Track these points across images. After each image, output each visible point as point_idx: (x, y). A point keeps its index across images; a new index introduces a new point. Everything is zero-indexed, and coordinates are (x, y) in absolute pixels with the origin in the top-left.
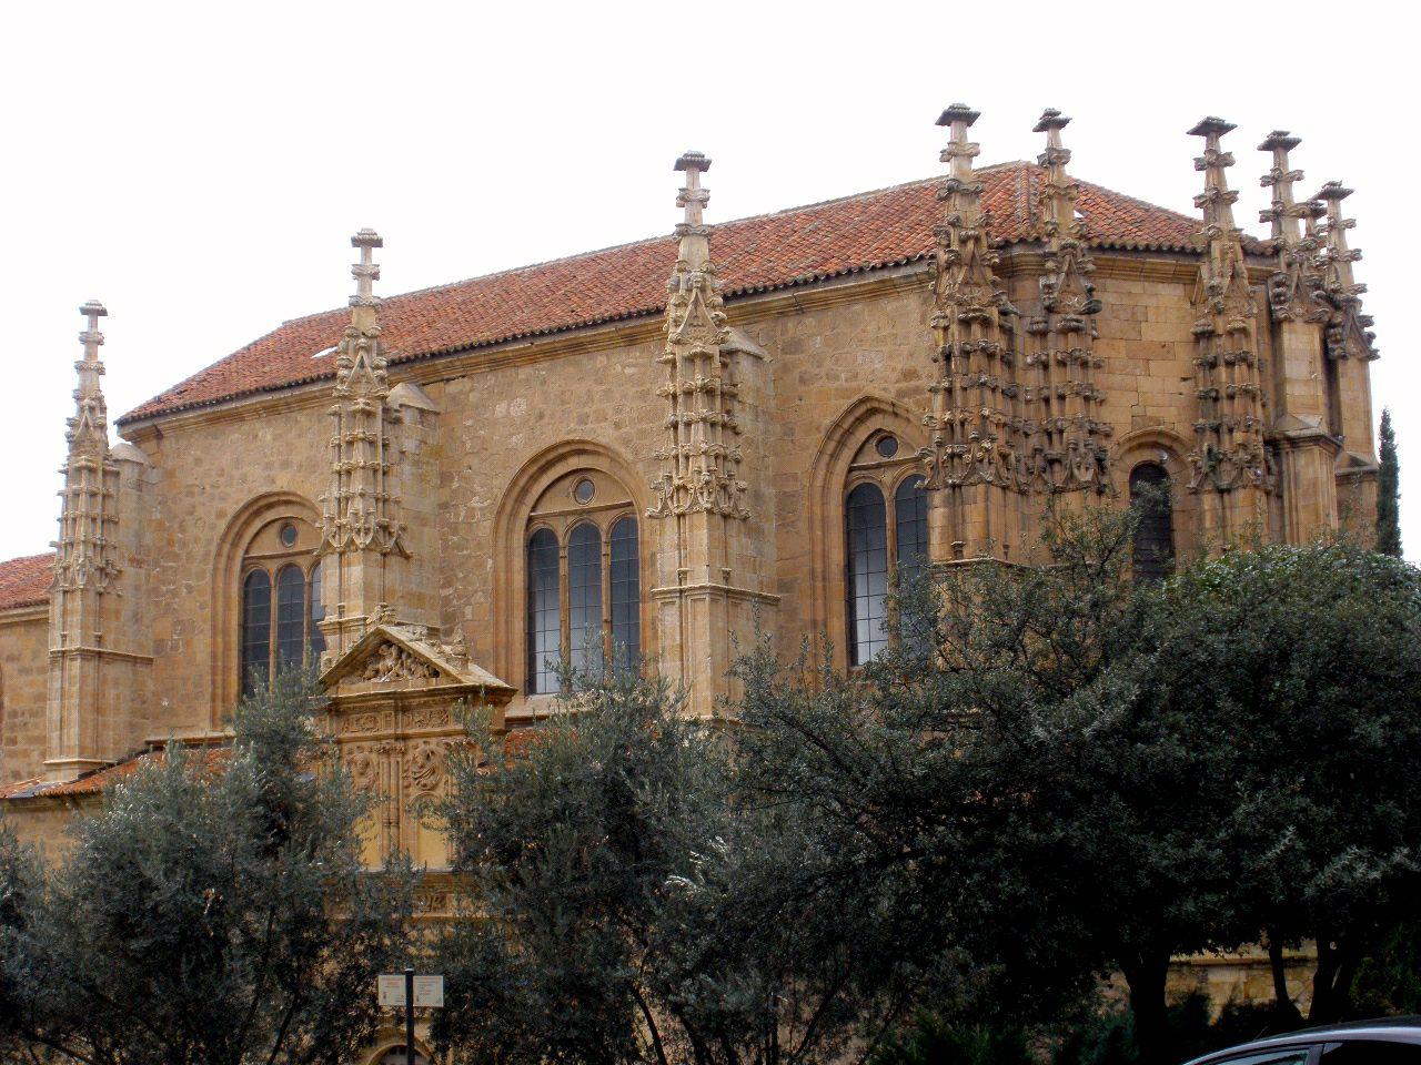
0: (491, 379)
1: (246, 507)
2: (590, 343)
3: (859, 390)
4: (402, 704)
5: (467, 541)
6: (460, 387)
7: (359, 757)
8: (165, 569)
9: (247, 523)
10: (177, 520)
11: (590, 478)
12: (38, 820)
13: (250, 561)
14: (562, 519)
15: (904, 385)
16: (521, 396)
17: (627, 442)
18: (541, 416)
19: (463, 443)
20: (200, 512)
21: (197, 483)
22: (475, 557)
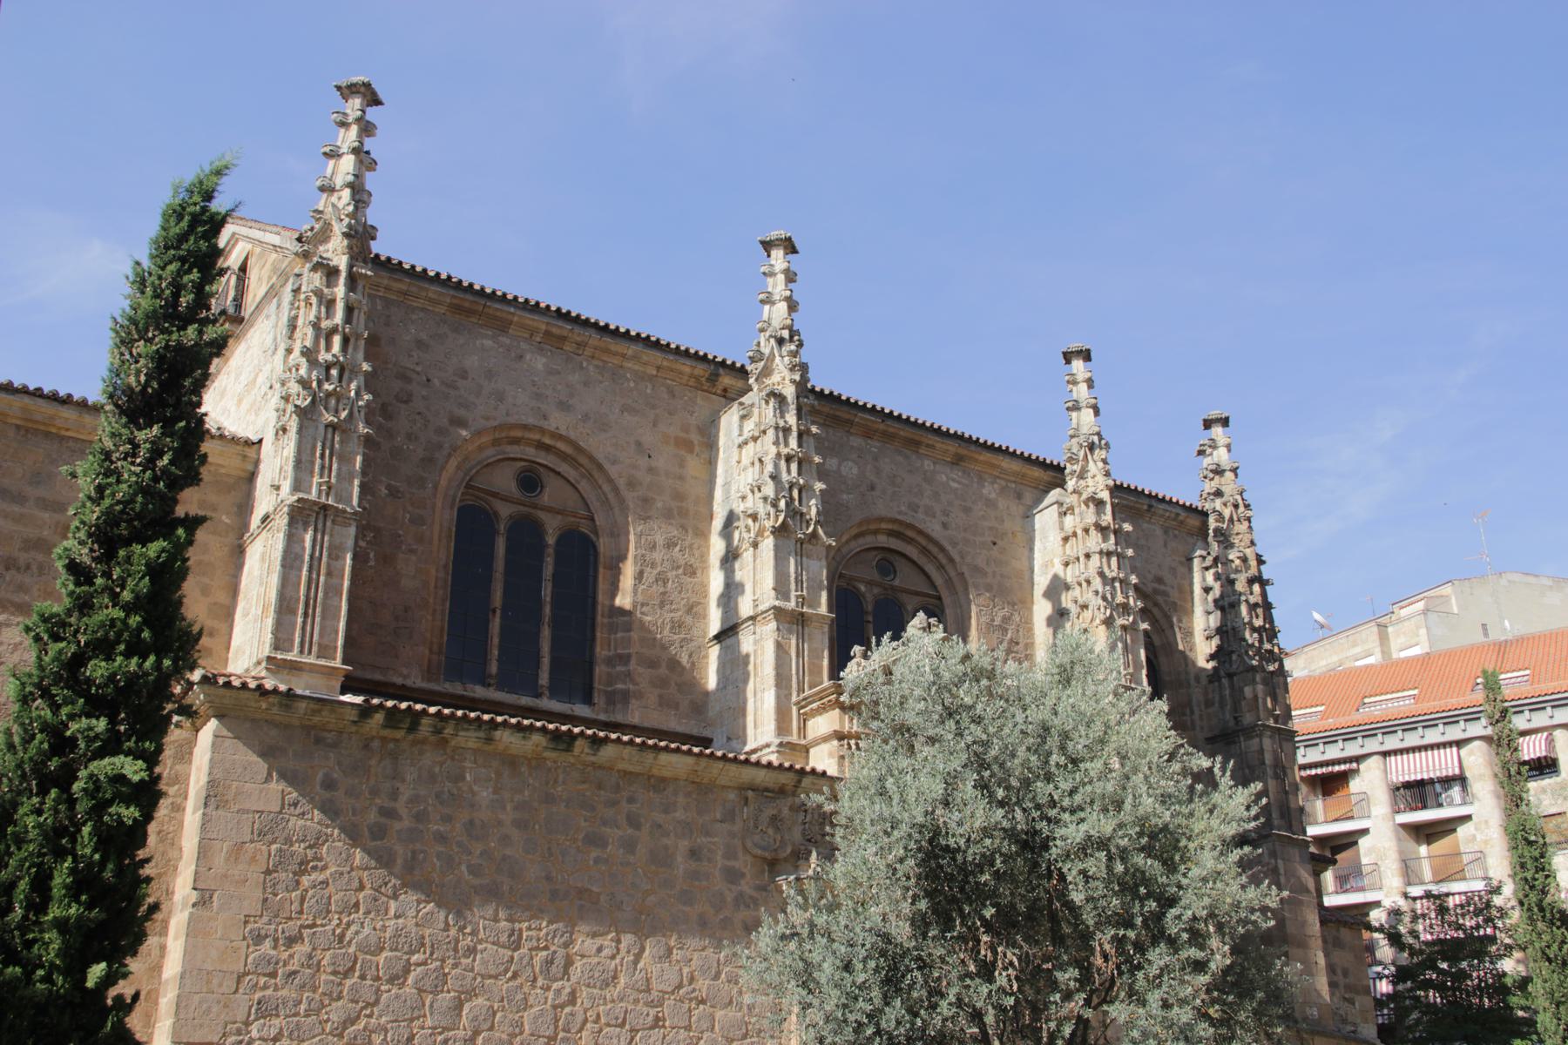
11: (896, 564)
15: (1156, 585)
16: (854, 461)
18: (872, 488)
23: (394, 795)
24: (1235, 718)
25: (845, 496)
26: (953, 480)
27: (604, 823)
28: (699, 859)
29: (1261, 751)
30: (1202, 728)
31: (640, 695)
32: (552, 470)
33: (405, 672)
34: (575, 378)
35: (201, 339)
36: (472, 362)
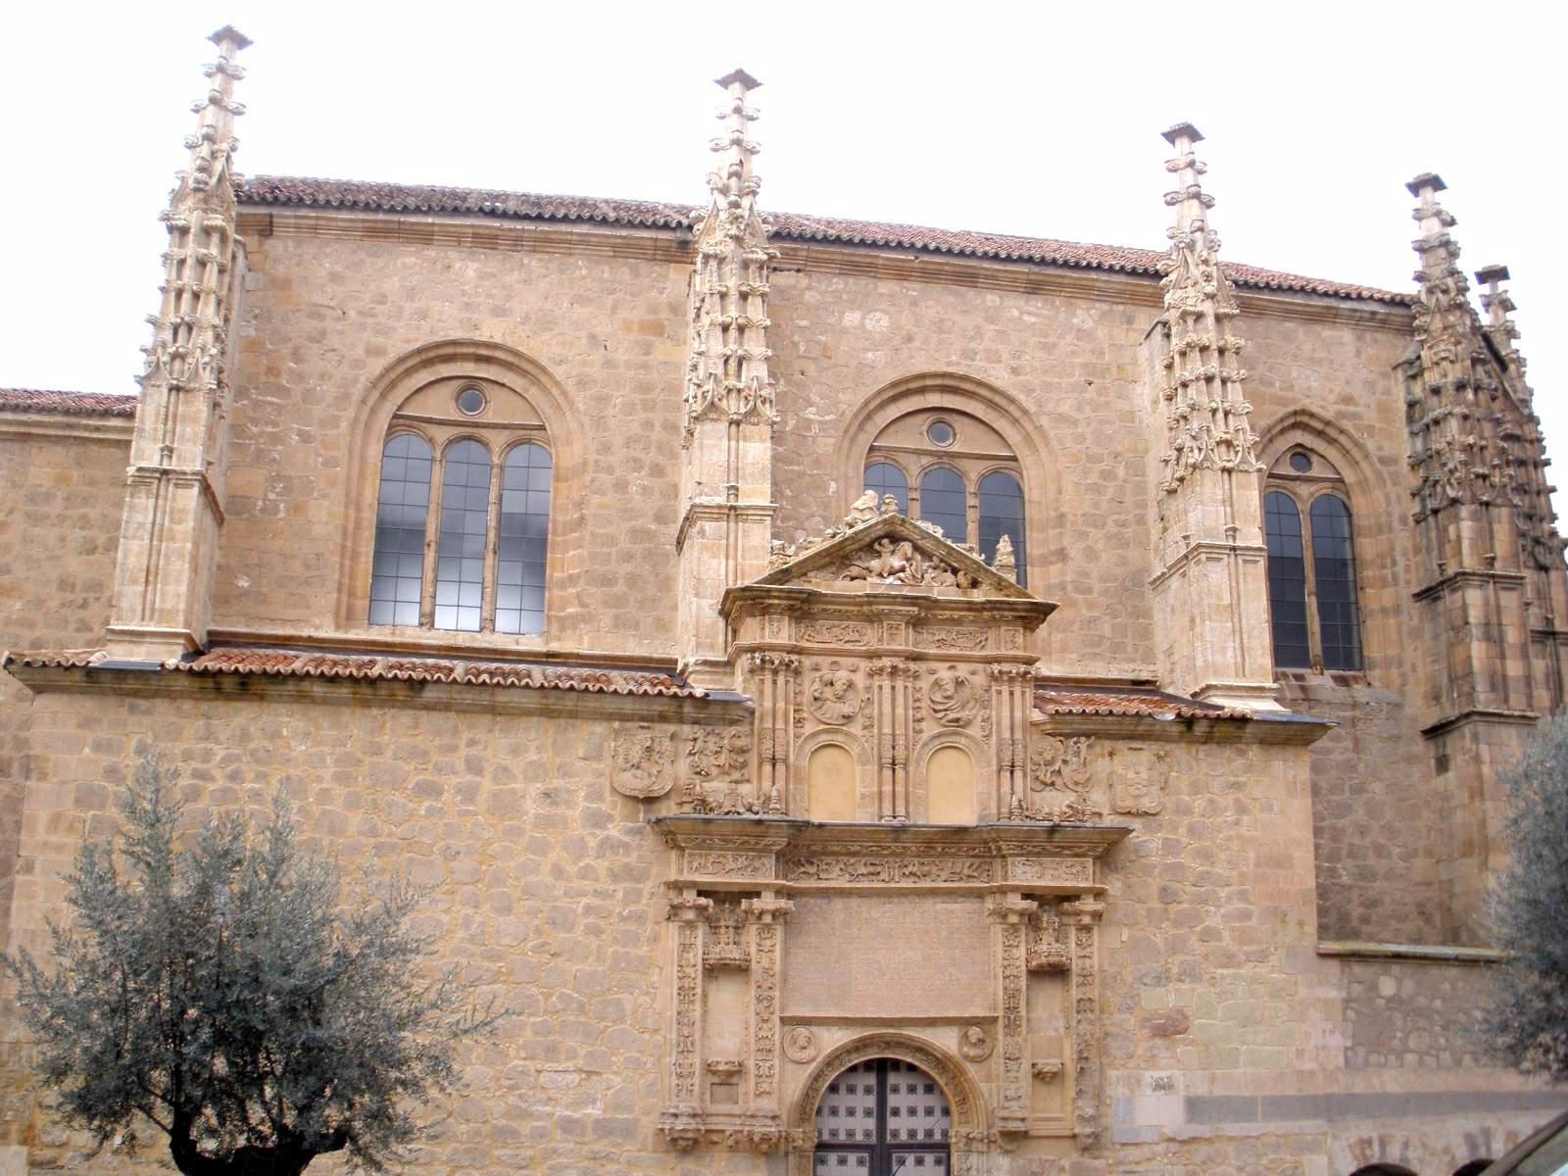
0: (838, 283)
1: (419, 351)
2: (986, 277)
3: (1294, 401)
4: (923, 613)
5: (800, 455)
6: (792, 281)
7: (842, 675)
8: (257, 405)
9: (409, 372)
10: (290, 345)
11: (956, 426)
12: (132, 709)
13: (401, 421)
14: (914, 457)
15: (1342, 407)
16: (882, 311)
17: (1029, 391)
18: (910, 339)
19: (795, 345)
20: (332, 340)
21: (332, 304)
22: (811, 476)
23: (207, 756)
24: (1440, 566)
25: (870, 355)
28: (554, 803)
29: (1464, 607)
30: (1408, 582)
32: (496, 382)
33: (317, 621)
34: (514, 277)
36: (392, 285)
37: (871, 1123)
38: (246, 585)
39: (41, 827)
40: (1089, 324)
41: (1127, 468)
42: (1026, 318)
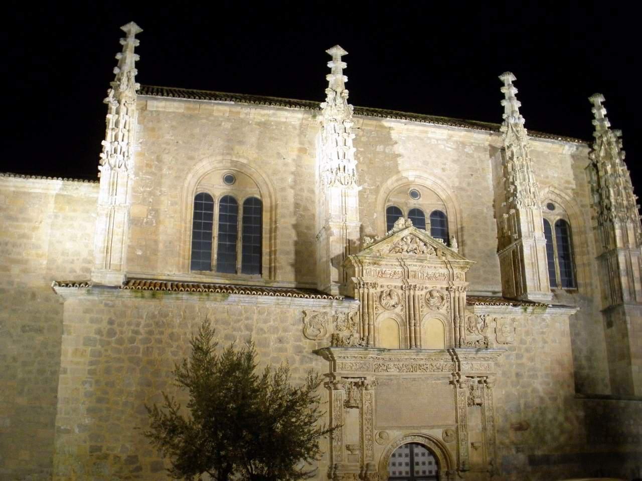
15: (567, 185)
25: (388, 163)
26: (448, 147)
27: (235, 330)
30: (593, 253)
31: (281, 268)
35: (366, 236)
37: (408, 469)
38: (140, 254)
39: (69, 354)
40: (471, 152)
41: (487, 208)
42: (447, 149)
